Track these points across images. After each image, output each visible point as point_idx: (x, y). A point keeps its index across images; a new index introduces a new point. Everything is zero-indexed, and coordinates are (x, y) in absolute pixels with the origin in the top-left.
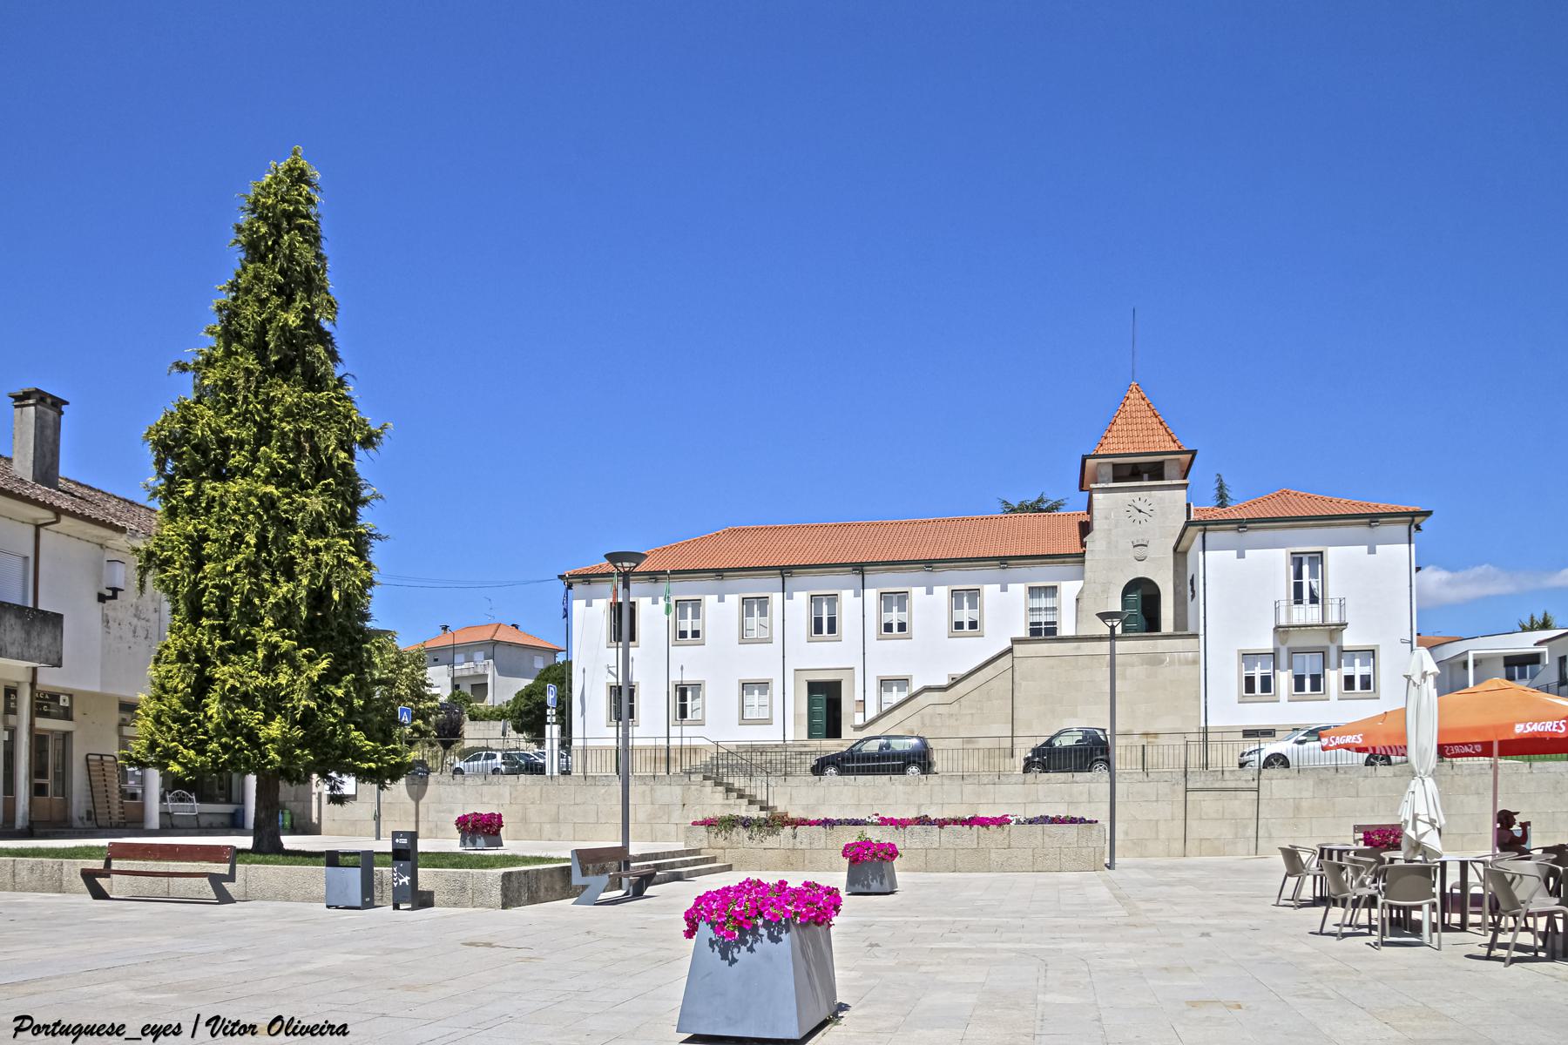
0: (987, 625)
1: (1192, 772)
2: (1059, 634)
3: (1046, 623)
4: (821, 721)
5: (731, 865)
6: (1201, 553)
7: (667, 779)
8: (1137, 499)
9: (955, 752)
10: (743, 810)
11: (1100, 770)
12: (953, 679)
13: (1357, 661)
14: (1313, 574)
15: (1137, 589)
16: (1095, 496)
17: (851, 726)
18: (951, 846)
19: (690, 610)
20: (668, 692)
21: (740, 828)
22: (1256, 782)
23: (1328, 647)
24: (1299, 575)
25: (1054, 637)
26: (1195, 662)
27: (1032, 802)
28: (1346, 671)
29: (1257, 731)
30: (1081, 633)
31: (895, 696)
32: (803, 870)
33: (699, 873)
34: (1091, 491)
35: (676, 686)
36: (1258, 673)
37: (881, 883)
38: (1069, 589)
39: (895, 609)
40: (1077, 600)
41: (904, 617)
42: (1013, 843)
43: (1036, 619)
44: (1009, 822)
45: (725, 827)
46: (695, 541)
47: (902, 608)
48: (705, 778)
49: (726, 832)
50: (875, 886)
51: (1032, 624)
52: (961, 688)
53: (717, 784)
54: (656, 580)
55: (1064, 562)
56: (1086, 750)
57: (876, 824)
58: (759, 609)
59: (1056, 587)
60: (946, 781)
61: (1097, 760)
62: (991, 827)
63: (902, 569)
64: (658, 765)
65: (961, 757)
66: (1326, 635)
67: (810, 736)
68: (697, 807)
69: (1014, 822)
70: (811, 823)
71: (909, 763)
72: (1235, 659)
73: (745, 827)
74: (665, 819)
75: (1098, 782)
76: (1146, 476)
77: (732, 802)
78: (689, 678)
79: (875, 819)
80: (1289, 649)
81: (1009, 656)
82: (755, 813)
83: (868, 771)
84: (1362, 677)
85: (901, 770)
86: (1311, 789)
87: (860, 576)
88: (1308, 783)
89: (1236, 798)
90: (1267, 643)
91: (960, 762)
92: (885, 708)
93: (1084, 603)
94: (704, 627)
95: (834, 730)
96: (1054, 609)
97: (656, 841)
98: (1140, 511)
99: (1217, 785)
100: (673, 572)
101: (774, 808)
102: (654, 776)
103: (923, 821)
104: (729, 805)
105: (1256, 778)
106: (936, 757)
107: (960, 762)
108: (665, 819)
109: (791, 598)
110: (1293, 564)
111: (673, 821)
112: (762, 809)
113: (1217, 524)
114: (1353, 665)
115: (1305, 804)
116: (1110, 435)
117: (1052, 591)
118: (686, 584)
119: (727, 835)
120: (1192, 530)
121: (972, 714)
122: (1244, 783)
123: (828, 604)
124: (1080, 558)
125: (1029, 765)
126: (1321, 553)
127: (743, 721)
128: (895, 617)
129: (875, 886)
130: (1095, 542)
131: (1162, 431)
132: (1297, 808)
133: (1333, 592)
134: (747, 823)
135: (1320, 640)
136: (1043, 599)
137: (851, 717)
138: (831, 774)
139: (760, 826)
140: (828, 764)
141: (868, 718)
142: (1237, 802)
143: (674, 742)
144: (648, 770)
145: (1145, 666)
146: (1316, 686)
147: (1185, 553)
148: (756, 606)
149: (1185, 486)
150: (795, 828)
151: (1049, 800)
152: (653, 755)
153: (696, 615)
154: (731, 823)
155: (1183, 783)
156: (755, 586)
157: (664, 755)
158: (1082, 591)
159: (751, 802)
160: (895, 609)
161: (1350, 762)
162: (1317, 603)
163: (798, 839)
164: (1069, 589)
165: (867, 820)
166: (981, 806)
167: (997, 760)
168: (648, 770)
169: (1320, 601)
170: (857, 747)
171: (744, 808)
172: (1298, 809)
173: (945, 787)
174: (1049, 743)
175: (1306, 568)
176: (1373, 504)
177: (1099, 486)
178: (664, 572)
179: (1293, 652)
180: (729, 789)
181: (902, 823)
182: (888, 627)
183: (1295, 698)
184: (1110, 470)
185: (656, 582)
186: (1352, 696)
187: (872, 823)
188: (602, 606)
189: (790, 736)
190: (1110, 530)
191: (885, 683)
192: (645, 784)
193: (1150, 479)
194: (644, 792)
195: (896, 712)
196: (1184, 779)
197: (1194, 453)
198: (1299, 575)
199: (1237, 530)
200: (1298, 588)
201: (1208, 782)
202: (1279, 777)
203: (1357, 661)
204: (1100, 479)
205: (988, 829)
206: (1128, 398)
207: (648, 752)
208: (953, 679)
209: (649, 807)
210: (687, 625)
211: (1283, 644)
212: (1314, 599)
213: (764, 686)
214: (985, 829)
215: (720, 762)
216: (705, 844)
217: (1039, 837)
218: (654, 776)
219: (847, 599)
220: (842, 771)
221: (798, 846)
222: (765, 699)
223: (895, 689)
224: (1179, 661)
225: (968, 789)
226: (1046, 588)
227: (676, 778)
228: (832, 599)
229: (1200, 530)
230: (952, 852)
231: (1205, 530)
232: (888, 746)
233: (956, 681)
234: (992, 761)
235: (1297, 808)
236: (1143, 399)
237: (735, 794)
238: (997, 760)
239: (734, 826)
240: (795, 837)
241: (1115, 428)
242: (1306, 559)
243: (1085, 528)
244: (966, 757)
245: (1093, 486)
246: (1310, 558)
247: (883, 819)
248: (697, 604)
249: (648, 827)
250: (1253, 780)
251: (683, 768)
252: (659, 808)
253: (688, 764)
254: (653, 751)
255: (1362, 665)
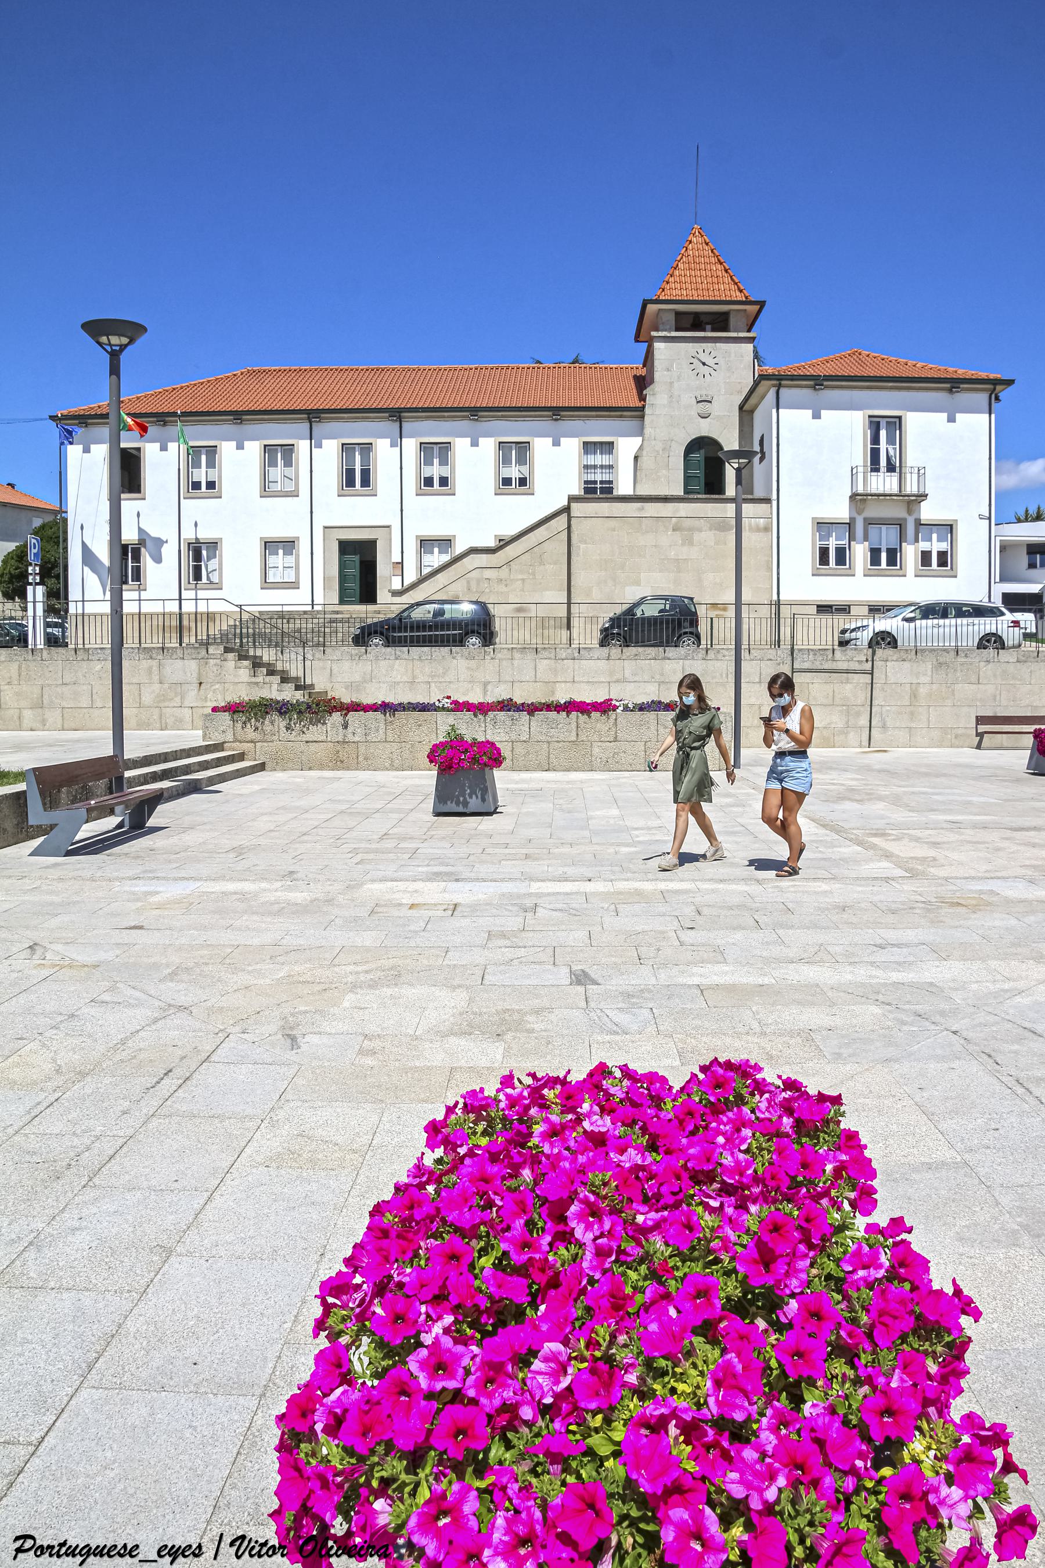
0: (539, 481)
1: (800, 650)
2: (615, 493)
3: (602, 482)
4: (354, 586)
5: (264, 764)
6: (774, 411)
7: (180, 653)
8: (701, 351)
9: (509, 620)
10: (275, 691)
11: (688, 645)
12: (500, 540)
13: (935, 536)
14: (891, 441)
15: (700, 448)
16: (658, 346)
17: (389, 591)
18: (543, 738)
19: (204, 458)
20: (180, 551)
21: (275, 716)
22: (870, 663)
23: (905, 520)
24: (876, 440)
25: (610, 496)
26: (767, 529)
27: (617, 681)
28: (924, 546)
29: (831, 606)
30: (644, 490)
31: (436, 559)
32: (357, 769)
33: (223, 778)
34: (650, 341)
35: (189, 544)
36: (832, 544)
37: (483, 800)
38: (627, 447)
39: (436, 461)
40: (636, 458)
41: (445, 471)
42: (620, 735)
43: (591, 477)
44: (615, 708)
45: (256, 714)
46: (209, 381)
47: (444, 462)
48: (227, 650)
49: (257, 720)
50: (474, 803)
51: (586, 482)
52: (510, 551)
53: (241, 657)
54: (165, 424)
55: (621, 416)
56: (673, 620)
57: (448, 710)
58: (283, 458)
59: (613, 443)
60: (517, 655)
61: (686, 633)
62: (593, 714)
63: (444, 417)
64: (167, 635)
65: (509, 627)
66: (905, 506)
67: (342, 602)
68: (217, 686)
69: (621, 708)
70: (367, 708)
71: (467, 634)
72: (808, 528)
73: (281, 714)
74: (177, 701)
75: (693, 659)
76: (709, 327)
77: (260, 679)
78: (204, 534)
79: (447, 703)
80: (865, 519)
81: (565, 516)
82: (289, 694)
83: (424, 641)
84: (939, 552)
85: (460, 641)
86: (930, 673)
87: (398, 424)
88: (927, 666)
89: (847, 681)
90: (841, 511)
91: (509, 633)
92: (426, 571)
93: (644, 461)
94: (220, 477)
95: (368, 594)
96: (610, 467)
97: (166, 729)
98: (704, 364)
99: (827, 666)
100: (185, 414)
101: (312, 686)
102: (163, 649)
103: (506, 705)
104: (257, 683)
105: (870, 659)
106: (498, 625)
107: (509, 633)
108: (177, 701)
109: (319, 446)
110: (870, 428)
111: (187, 703)
112: (298, 688)
113: (792, 380)
114: (930, 540)
115: (923, 691)
116: (672, 280)
117: (608, 447)
118: (199, 428)
119: (259, 725)
120: (765, 384)
121: (523, 580)
122: (857, 664)
123: (361, 454)
124: (639, 413)
125: (607, 637)
126: (900, 418)
127: (266, 584)
128: (435, 471)
129: (474, 803)
130: (657, 398)
131: (727, 280)
132: (914, 695)
133: (913, 458)
134: (283, 709)
135: (897, 512)
136: (599, 456)
137: (387, 581)
138: (376, 646)
139: (300, 712)
140: (376, 632)
141: (406, 583)
142: (849, 686)
143: (188, 607)
144: (155, 640)
145: (713, 532)
146: (892, 561)
147: (752, 412)
148: (279, 455)
149: (751, 340)
150: (346, 715)
151: (636, 679)
152: (161, 623)
153: (211, 464)
154: (262, 709)
155: (789, 662)
156: (279, 433)
157: (175, 623)
158: (641, 448)
159: (285, 680)
160: (436, 461)
161: (947, 644)
162: (894, 471)
163: (350, 729)
164: (627, 447)
165: (437, 704)
166: (557, 685)
167: (552, 631)
168: (155, 640)
169: (898, 470)
170: (405, 614)
171: (275, 687)
172: (915, 697)
173: (516, 662)
174: (630, 611)
175: (883, 434)
176: (951, 369)
177: (661, 334)
178: (174, 414)
179: (869, 522)
180: (257, 663)
181: (481, 709)
182: (429, 482)
183: (872, 572)
184: (672, 317)
185: (165, 425)
186: (928, 573)
187: (443, 709)
188: (101, 451)
189: (319, 599)
190: (671, 383)
191: (426, 544)
192: (151, 658)
193: (713, 330)
194: (150, 668)
195: (439, 576)
196: (790, 658)
197: (762, 304)
198: (876, 440)
199: (814, 387)
200: (875, 454)
201: (818, 663)
202: (895, 658)
203: (935, 536)
204: (661, 327)
205: (590, 717)
206: (690, 242)
207: (155, 618)
208: (500, 540)
209: (156, 687)
210: (201, 475)
211: (859, 514)
212: (891, 468)
213: (289, 545)
214: (586, 716)
215: (244, 631)
216: (229, 737)
217: (653, 728)
218: (163, 649)
219: (384, 452)
220: (390, 642)
221: (350, 737)
222: (290, 560)
223: (436, 550)
224: (750, 525)
225: (543, 665)
226: (602, 443)
227: (189, 651)
228: (367, 449)
229: (774, 386)
230: (545, 746)
231: (779, 386)
232: (440, 613)
233: (504, 543)
234: (546, 632)
235: (914, 695)
236: (707, 244)
237: (264, 670)
238: (552, 631)
239: (267, 713)
240: (345, 726)
241: (677, 272)
242: (883, 423)
243: (642, 383)
244: (515, 626)
245: (654, 334)
246: (887, 422)
247: (455, 702)
248: (212, 452)
249: (156, 711)
250: (867, 661)
251: (199, 637)
252: (170, 688)
253: (205, 634)
254: (161, 618)
255: (939, 540)
